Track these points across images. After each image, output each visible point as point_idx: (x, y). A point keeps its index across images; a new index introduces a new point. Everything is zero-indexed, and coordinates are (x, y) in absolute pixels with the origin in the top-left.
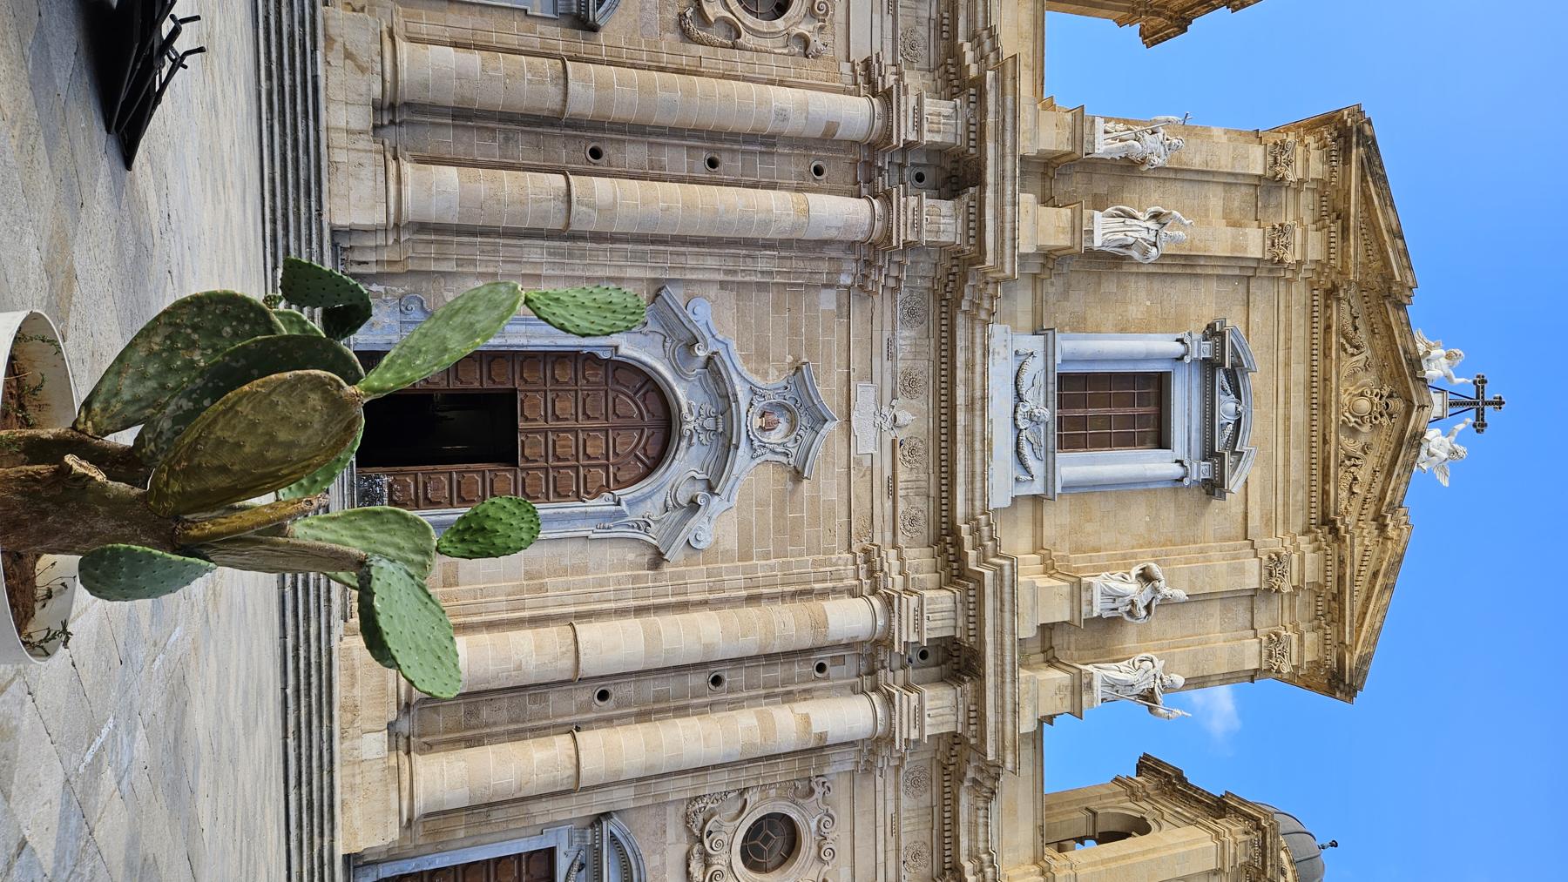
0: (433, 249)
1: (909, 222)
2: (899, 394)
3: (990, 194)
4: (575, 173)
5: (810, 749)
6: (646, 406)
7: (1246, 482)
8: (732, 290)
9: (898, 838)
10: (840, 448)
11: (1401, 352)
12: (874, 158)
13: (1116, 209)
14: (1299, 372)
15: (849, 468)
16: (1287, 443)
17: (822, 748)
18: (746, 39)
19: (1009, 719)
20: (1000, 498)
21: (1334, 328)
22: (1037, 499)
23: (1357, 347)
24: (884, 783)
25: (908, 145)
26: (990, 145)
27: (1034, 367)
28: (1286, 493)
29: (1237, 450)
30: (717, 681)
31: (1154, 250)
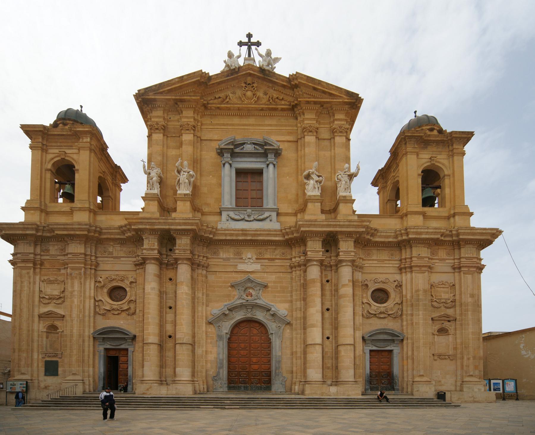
0: (199, 374)
1: (184, 253)
2: (241, 257)
3: (173, 227)
4: (175, 342)
5: (353, 285)
6: (244, 326)
7: (277, 141)
8: (209, 304)
9: (385, 260)
10: (258, 275)
11: (228, 78)
12: (165, 263)
13: (177, 185)
14: (236, 120)
15: (265, 272)
16: (262, 125)
17: (353, 281)
18: (133, 298)
19: (352, 223)
20: (277, 226)
21: (219, 106)
22: (278, 214)
23: (227, 97)
24: (367, 264)
25: (160, 252)
26: (156, 227)
27: (232, 214)
28: (281, 126)
29: (264, 144)
30: (328, 310)
31: (190, 173)
